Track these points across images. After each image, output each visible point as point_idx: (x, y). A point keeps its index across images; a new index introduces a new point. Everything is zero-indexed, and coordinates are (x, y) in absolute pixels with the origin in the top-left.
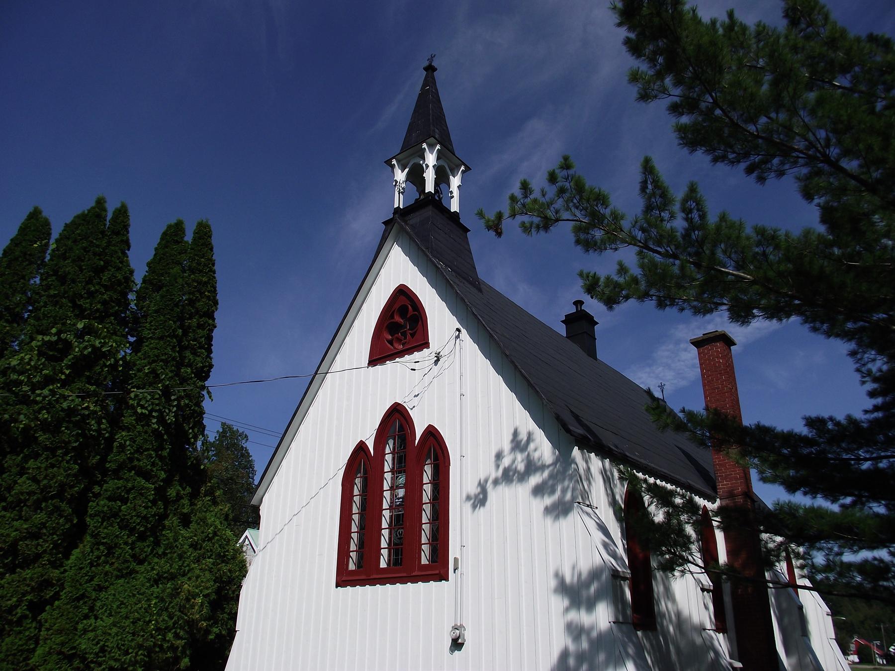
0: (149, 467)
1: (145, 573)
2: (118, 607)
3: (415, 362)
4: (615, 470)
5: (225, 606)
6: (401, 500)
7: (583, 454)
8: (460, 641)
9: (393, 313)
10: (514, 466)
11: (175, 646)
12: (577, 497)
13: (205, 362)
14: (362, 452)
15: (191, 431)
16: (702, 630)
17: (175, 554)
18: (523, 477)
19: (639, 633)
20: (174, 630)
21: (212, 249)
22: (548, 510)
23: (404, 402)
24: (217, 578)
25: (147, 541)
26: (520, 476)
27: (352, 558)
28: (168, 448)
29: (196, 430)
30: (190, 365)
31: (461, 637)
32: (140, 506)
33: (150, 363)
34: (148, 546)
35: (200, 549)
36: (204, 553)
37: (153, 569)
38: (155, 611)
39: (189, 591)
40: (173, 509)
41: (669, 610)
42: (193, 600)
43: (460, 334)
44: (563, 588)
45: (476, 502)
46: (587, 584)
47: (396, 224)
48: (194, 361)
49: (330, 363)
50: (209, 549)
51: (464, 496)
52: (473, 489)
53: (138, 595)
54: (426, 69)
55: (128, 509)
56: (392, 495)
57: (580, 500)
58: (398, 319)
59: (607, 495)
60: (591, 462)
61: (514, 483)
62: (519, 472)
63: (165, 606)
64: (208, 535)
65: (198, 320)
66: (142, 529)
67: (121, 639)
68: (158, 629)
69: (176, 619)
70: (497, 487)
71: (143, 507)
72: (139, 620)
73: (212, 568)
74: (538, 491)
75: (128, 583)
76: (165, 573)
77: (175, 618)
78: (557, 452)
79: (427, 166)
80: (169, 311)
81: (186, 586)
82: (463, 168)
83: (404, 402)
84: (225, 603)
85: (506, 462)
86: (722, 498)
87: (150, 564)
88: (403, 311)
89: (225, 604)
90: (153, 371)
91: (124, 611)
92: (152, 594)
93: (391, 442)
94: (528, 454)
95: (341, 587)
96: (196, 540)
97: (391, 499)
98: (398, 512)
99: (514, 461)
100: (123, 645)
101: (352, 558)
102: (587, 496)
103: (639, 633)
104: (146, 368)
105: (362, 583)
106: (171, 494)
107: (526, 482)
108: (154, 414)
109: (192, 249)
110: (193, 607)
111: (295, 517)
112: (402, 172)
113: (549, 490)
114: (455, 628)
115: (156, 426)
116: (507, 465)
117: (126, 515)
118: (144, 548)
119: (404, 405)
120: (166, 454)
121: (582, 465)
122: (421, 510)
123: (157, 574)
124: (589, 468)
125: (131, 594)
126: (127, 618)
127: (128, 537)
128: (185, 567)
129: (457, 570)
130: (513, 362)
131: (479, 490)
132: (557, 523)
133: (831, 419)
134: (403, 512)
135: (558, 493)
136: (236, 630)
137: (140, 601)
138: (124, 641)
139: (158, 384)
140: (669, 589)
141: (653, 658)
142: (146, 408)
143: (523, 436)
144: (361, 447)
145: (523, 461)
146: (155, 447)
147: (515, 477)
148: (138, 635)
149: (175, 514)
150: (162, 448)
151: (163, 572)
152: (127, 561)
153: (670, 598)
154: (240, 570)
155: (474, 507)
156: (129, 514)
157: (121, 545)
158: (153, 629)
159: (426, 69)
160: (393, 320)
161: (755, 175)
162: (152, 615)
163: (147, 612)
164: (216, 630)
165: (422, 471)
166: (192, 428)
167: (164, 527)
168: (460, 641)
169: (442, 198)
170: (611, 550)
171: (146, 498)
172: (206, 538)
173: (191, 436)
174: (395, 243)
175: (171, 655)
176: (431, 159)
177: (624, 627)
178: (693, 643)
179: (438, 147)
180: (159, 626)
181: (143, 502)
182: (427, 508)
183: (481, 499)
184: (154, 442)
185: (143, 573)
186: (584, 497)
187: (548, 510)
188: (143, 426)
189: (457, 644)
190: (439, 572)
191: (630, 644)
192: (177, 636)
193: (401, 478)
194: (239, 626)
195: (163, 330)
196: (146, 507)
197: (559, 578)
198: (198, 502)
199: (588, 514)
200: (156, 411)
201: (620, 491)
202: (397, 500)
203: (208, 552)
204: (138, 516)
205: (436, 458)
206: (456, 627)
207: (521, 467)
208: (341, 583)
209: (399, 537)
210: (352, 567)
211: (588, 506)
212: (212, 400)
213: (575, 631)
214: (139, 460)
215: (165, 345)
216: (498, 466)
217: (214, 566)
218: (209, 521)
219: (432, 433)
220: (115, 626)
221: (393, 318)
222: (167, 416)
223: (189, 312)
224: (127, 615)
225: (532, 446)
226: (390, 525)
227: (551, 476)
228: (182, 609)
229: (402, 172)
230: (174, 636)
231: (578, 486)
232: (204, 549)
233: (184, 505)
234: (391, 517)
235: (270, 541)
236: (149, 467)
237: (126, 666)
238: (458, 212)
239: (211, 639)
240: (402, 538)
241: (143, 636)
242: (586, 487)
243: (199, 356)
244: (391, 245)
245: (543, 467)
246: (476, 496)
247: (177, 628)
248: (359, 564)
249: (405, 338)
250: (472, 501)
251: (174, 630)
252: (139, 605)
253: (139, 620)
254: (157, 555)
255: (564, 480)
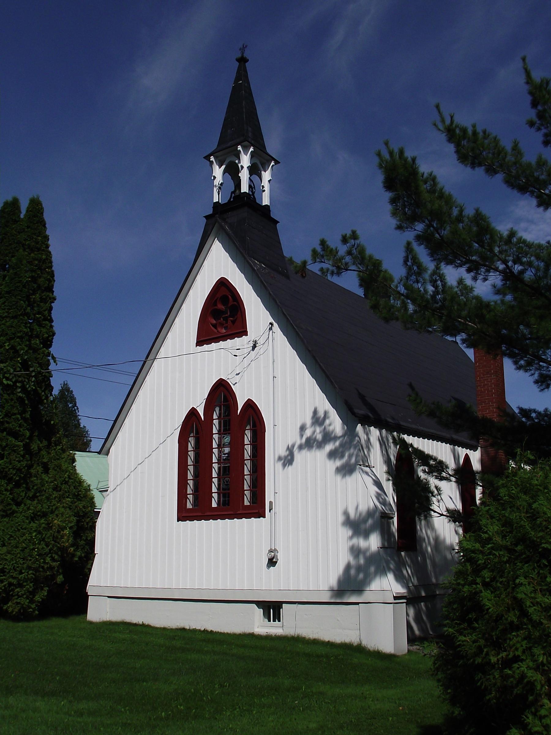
0: (17, 428)
1: (23, 513)
2: (9, 539)
3: (237, 349)
4: (389, 436)
5: (82, 534)
6: (227, 455)
7: (364, 429)
8: (274, 560)
9: (216, 301)
10: (314, 436)
11: (52, 566)
12: (359, 461)
13: (49, 332)
14: (194, 416)
15: (43, 393)
16: (452, 550)
17: (44, 497)
18: (320, 445)
19: (403, 553)
20: (50, 555)
21: (44, 225)
22: (338, 470)
23: (228, 379)
24: (75, 513)
25: (21, 487)
26: (318, 444)
27: (189, 499)
28: (29, 410)
29: (47, 392)
30: (37, 336)
31: (275, 557)
32: (14, 460)
33: (9, 340)
34: (23, 491)
35: (60, 491)
36: (63, 494)
37: (29, 509)
38: (36, 541)
39: (59, 525)
40: (37, 460)
41: (428, 535)
42: (62, 532)
43: (273, 327)
44: (348, 522)
45: (286, 462)
46: (365, 521)
47: (217, 225)
48: (40, 333)
49: (162, 340)
50: (67, 491)
51: (277, 457)
52: (283, 452)
53: (22, 529)
54: (238, 60)
55: (5, 464)
56: (220, 452)
57: (361, 463)
58: (221, 307)
59: (383, 455)
60: (370, 433)
61: (314, 448)
62: (318, 441)
63: (42, 538)
64: (65, 479)
65: (40, 295)
66: (17, 478)
67: (15, 563)
68: (39, 555)
69: (52, 546)
70: (301, 451)
71: (17, 461)
72: (26, 548)
73: (71, 506)
74: (332, 455)
75: (12, 520)
76: (39, 512)
77: (51, 546)
78: (346, 428)
79: (242, 167)
80: (19, 292)
81: (56, 521)
82: (273, 163)
83: (228, 379)
84: (82, 532)
85: (308, 433)
86: (483, 446)
87: (25, 505)
88: (224, 300)
89: (82, 533)
90: (13, 347)
91: (13, 542)
92: (31, 529)
93: (217, 409)
94: (325, 428)
95: (182, 521)
96: (57, 484)
97: (218, 454)
98: (225, 464)
99: (314, 432)
100: (18, 567)
101: (189, 499)
102: (366, 459)
103: (403, 553)
104: (7, 344)
105: (199, 518)
106: (34, 448)
107: (323, 448)
108: (18, 385)
109: (28, 227)
110: (62, 537)
111: (140, 465)
112: (220, 168)
113: (340, 455)
114: (271, 551)
115: (20, 394)
116: (308, 435)
117: (4, 468)
118: (20, 493)
119: (228, 381)
120: (28, 416)
121: (363, 436)
122: (243, 464)
123: (33, 513)
124: (369, 439)
125: (16, 529)
126: (17, 547)
127: (7, 486)
128: (53, 506)
129: (271, 511)
130: (314, 357)
131: (288, 452)
132: (344, 480)
133: (535, 411)
134: (229, 465)
135: (346, 458)
136: (95, 553)
137: (24, 534)
138: (18, 564)
139: (18, 358)
140: (430, 521)
141: (413, 571)
142: (11, 380)
143: (321, 414)
144: (193, 412)
145: (320, 432)
146: (20, 411)
147: (314, 445)
148: (27, 560)
149: (38, 464)
150: (24, 412)
151: (37, 511)
152: (9, 504)
153: (430, 527)
154: (91, 506)
155: (284, 465)
156: (7, 467)
157: (3, 492)
158: (37, 555)
159: (238, 60)
160: (216, 307)
161: (472, 274)
162: (34, 544)
163: (30, 542)
164: (78, 554)
165: (243, 434)
166: (44, 391)
167: (31, 476)
168: (274, 560)
169: (255, 192)
170: (382, 498)
171: (18, 454)
172: (63, 481)
173: (44, 398)
174: (216, 239)
175: (50, 573)
176: (245, 161)
177: (389, 550)
178: (445, 558)
179: (252, 149)
180: (40, 552)
181: (16, 457)
182: (248, 463)
183: (289, 460)
184: (18, 407)
185: (21, 512)
186: (364, 460)
187: (338, 470)
188: (9, 395)
189: (272, 562)
190: (259, 511)
191: (392, 562)
192: (53, 560)
193: (226, 438)
194: (97, 550)
195: (16, 309)
196: (19, 461)
197: (346, 513)
198: (51, 451)
199: (367, 473)
200: (19, 382)
201: (393, 451)
202: (224, 456)
203: (66, 493)
204: (14, 469)
205: (254, 425)
206: (272, 550)
207: (319, 437)
208: (181, 518)
209: (226, 483)
210: (189, 506)
211: (367, 466)
212: (57, 364)
213: (356, 551)
214: (8, 423)
215: (19, 324)
216: (302, 436)
217: (72, 504)
218: (64, 468)
219: (250, 405)
220: (9, 553)
221: (216, 305)
222: (27, 385)
223: (33, 289)
224: (16, 545)
225: (327, 422)
226: (219, 474)
227: (341, 445)
228: (55, 539)
229: (220, 168)
230: (50, 560)
231: (360, 453)
232: (63, 491)
233: (43, 456)
234: (219, 468)
235: (119, 484)
236: (17, 428)
237: (21, 582)
238: (269, 205)
239: (76, 561)
240: (228, 484)
241: (30, 560)
242: (366, 453)
243: (44, 327)
244: (213, 240)
245: (335, 438)
246: (286, 457)
247: (52, 553)
248: (195, 503)
249: (227, 323)
250: (282, 461)
251: (50, 555)
252: (24, 537)
253: (26, 548)
254: (29, 498)
255: (350, 448)
